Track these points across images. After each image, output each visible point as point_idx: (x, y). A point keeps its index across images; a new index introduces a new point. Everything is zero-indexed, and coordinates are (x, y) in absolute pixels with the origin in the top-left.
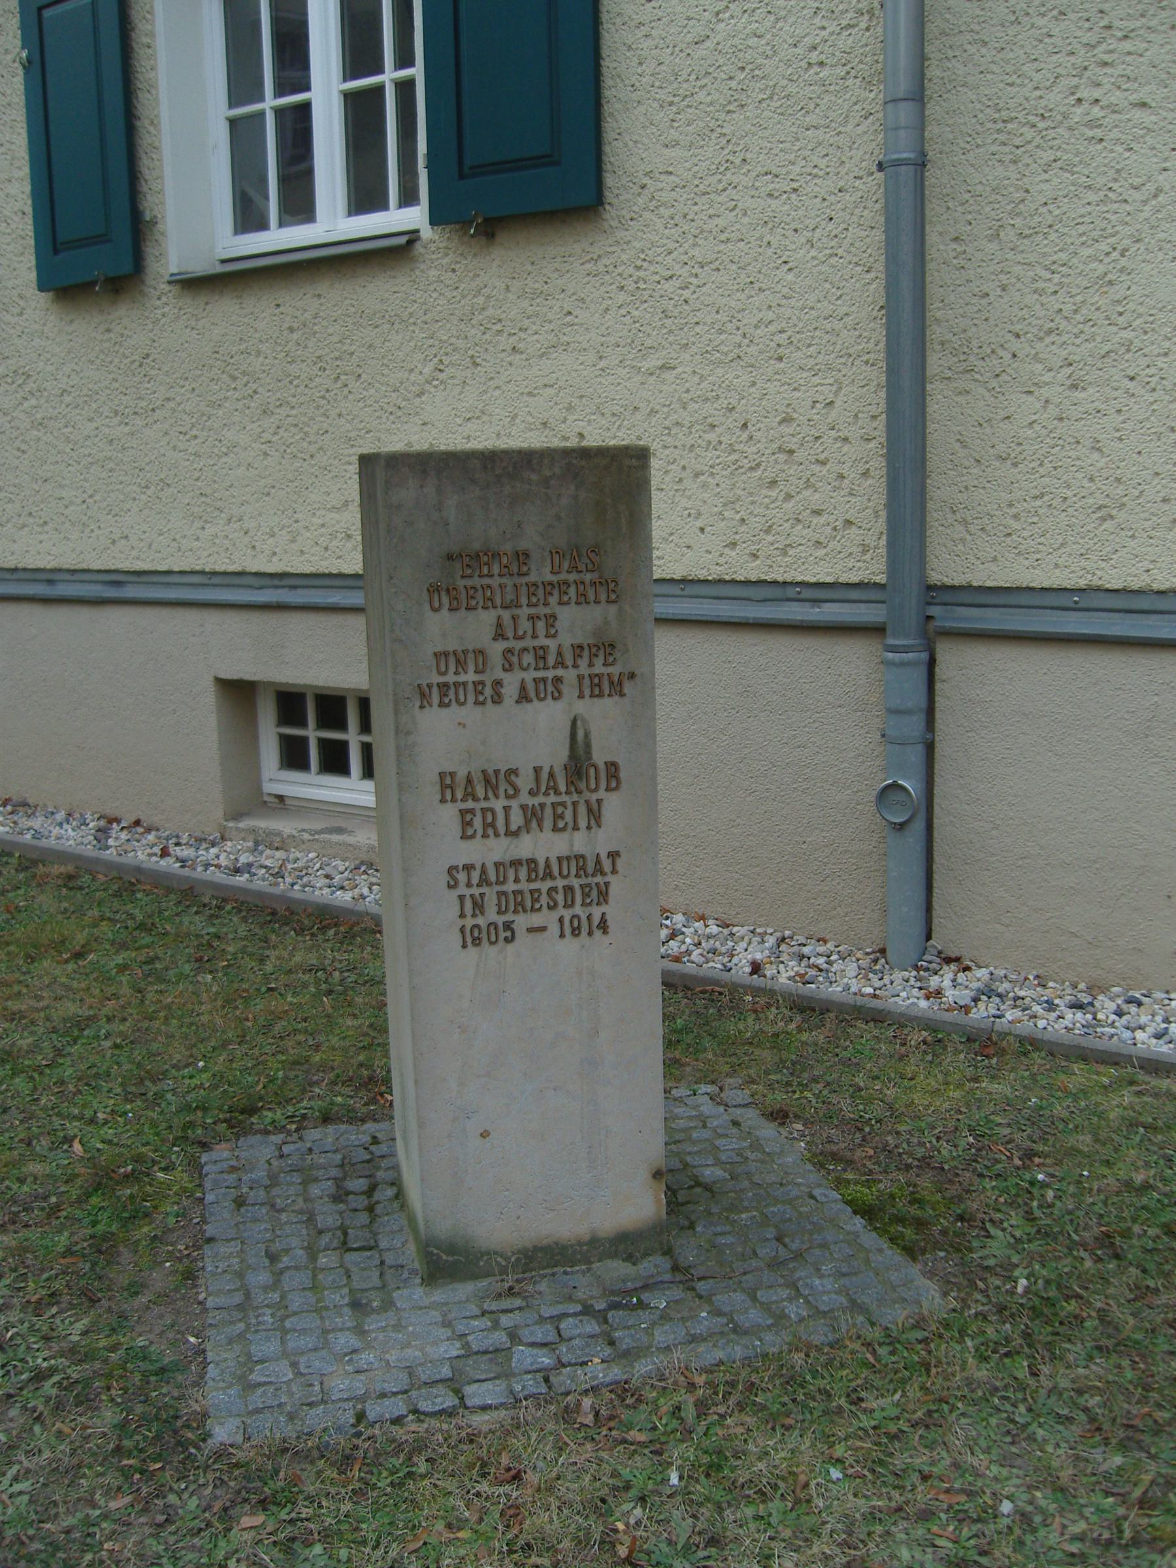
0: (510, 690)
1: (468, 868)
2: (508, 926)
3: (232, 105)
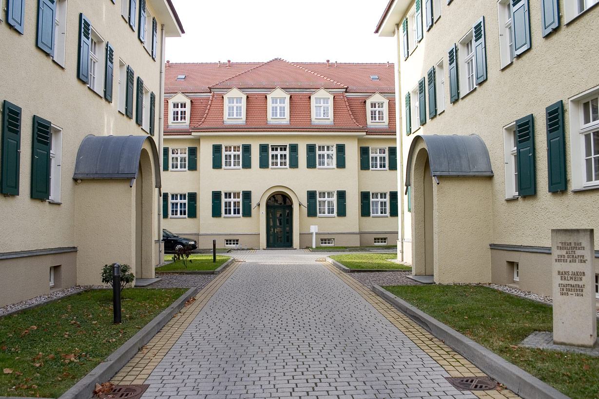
0: (568, 261)
1: (562, 284)
2: (567, 293)
3: (586, 157)
